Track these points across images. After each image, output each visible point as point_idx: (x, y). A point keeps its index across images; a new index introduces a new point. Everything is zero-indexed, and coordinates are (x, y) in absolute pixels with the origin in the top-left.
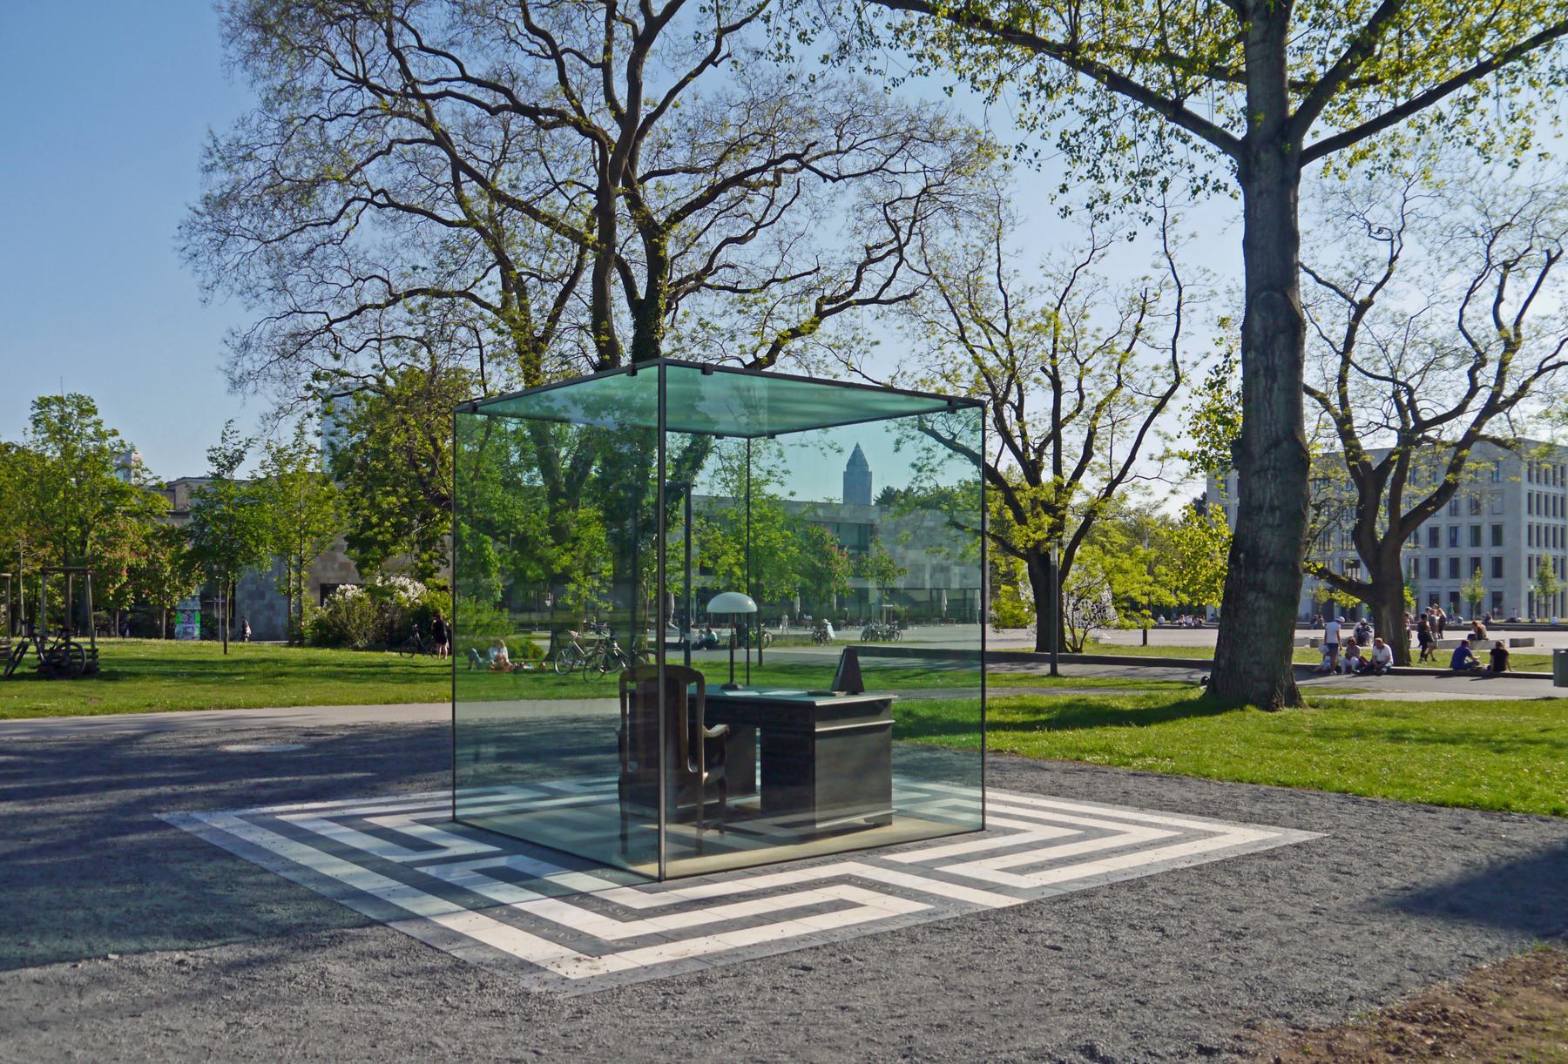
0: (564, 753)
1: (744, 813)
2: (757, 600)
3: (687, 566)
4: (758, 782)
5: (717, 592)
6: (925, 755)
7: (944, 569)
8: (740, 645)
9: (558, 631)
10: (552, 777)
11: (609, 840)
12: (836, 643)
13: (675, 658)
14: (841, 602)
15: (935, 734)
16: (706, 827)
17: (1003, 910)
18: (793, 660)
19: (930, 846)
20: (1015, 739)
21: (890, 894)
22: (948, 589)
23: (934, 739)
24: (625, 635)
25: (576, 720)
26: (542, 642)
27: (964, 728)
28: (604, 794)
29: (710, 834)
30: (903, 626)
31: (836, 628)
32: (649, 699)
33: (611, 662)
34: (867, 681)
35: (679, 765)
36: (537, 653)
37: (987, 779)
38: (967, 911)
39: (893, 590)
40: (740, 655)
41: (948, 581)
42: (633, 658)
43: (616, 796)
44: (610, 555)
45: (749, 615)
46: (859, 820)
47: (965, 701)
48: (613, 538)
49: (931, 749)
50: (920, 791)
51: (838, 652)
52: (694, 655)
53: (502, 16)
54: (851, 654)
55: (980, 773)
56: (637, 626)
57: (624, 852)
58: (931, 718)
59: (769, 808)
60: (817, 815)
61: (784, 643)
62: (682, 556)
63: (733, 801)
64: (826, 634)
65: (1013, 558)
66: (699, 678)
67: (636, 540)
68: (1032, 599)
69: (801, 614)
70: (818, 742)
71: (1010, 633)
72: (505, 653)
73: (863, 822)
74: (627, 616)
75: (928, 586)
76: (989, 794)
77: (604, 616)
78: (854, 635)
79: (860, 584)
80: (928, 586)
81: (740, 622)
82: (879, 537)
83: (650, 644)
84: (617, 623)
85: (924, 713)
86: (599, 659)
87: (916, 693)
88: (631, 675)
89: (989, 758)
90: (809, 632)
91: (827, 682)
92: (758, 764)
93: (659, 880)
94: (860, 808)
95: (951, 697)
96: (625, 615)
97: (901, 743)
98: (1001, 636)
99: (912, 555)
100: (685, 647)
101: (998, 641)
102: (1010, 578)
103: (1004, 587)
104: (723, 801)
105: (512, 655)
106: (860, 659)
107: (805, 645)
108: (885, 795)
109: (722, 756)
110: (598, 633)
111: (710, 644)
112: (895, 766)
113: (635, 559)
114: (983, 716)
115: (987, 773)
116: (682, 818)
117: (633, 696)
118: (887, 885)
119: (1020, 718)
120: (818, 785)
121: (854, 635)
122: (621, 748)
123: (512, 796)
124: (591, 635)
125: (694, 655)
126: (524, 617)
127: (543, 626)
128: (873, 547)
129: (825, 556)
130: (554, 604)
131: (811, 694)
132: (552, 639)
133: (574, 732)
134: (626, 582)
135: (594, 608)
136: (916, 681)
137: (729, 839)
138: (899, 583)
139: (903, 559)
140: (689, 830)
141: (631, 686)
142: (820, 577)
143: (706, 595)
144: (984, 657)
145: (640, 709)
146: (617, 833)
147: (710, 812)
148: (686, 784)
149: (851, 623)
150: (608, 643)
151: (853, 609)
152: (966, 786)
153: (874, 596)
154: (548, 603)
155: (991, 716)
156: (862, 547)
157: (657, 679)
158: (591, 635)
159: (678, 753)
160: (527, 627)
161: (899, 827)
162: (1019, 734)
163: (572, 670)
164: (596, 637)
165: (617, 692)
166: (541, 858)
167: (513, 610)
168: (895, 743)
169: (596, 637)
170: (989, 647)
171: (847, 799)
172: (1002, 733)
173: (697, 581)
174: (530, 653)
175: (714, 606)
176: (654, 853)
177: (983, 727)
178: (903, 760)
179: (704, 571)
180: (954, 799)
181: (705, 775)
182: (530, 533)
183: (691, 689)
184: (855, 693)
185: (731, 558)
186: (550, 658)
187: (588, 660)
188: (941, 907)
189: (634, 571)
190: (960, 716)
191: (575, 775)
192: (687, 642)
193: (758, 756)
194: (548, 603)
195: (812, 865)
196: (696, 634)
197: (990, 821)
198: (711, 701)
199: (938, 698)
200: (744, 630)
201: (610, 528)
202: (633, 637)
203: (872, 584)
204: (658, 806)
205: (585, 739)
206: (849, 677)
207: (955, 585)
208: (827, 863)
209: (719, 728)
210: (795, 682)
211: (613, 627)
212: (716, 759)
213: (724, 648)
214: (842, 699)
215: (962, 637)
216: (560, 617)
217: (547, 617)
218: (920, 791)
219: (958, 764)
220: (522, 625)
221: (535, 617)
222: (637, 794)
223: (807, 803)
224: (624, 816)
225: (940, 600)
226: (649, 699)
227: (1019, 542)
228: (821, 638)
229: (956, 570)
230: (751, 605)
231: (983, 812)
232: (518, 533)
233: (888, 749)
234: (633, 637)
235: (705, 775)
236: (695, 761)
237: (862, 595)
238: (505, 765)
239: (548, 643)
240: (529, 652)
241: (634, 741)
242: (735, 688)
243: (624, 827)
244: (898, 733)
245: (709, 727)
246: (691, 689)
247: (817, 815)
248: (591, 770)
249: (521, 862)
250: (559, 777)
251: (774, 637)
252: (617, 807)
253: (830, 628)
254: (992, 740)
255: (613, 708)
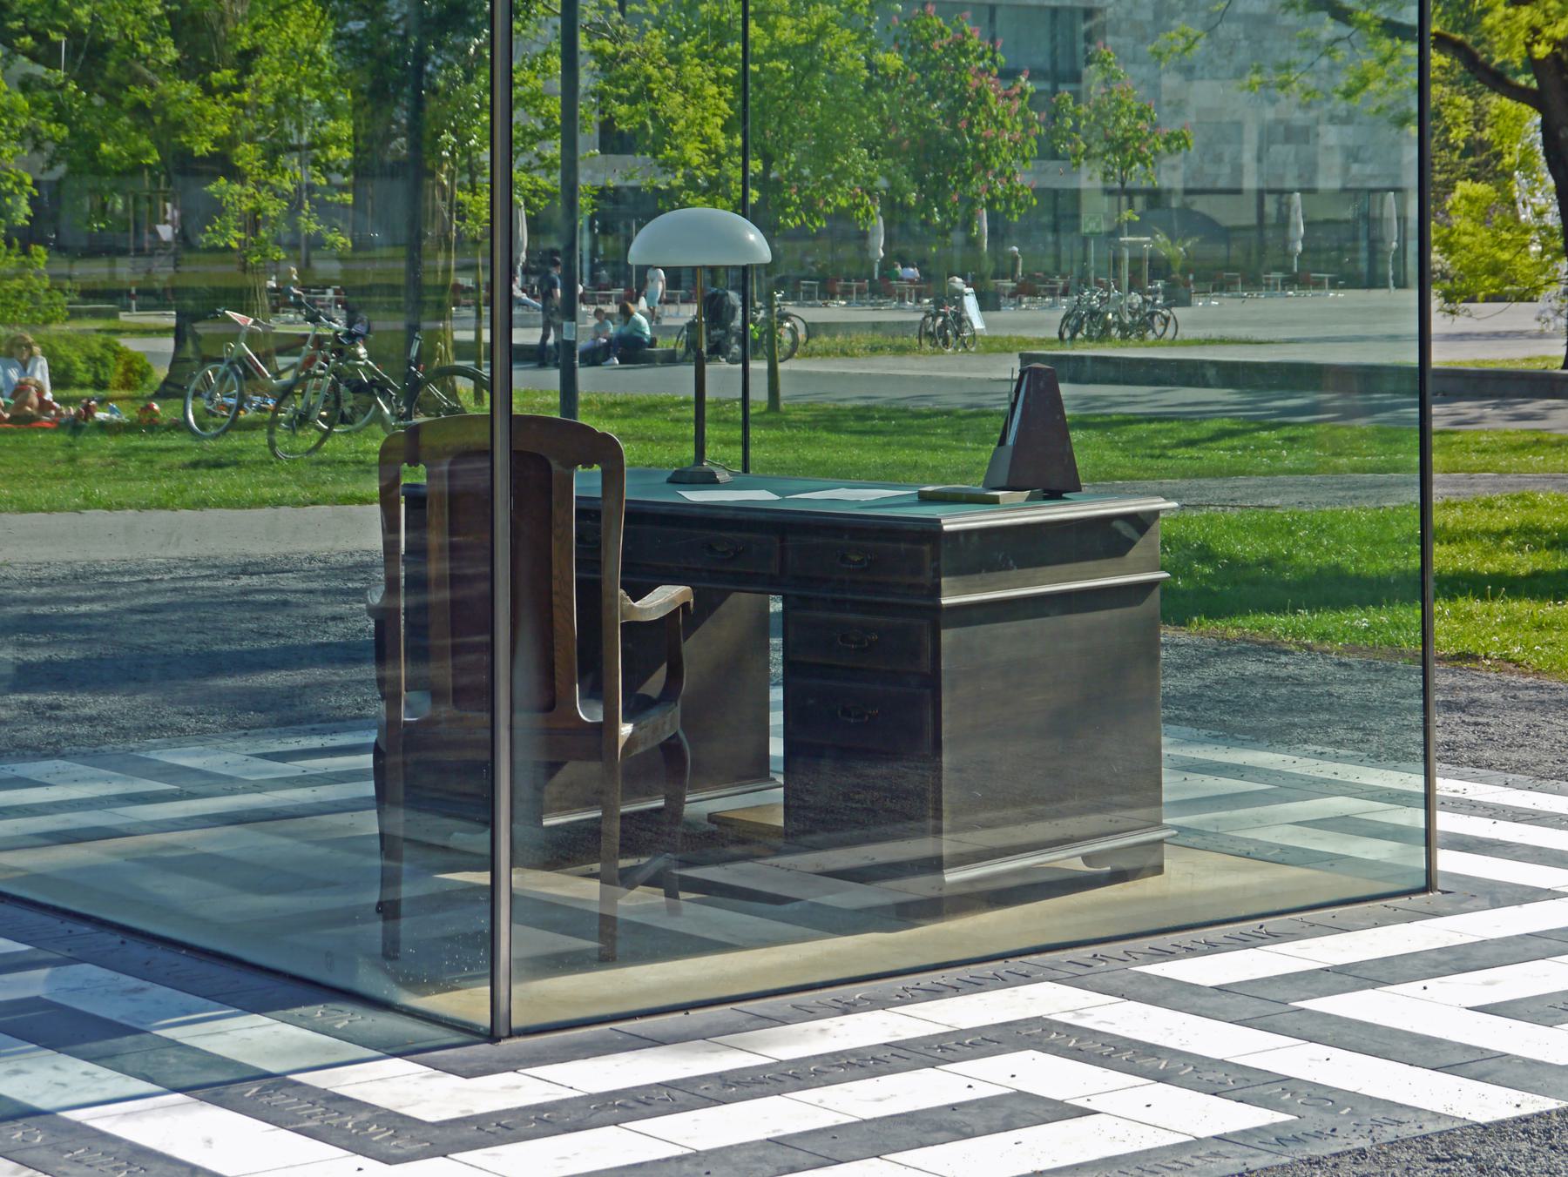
0: (213, 664)
1: (727, 838)
2: (769, 230)
3: (569, 130)
4: (776, 748)
5: (669, 199)
6: (1253, 667)
7: (1298, 135)
8: (717, 350)
9: (195, 310)
10: (178, 735)
11: (348, 917)
12: (993, 346)
13: (536, 391)
14: (998, 232)
15: (1279, 609)
16: (627, 879)
17: (1498, 1129)
18: (865, 408)
19: (1277, 937)
20: (1512, 623)
21: (1162, 1078)
22: (1308, 191)
23: (1278, 623)
24: (390, 323)
25: (246, 569)
26: (151, 343)
27: (1372, 592)
28: (321, 783)
29: (639, 902)
30: (1177, 297)
31: (987, 302)
32: (467, 508)
33: (350, 399)
34: (1087, 450)
35: (552, 703)
36: (134, 372)
37: (1439, 736)
38: (1390, 1133)
39: (1155, 197)
40: (722, 376)
41: (1310, 167)
42: (413, 393)
43: (369, 788)
44: (344, 98)
45: (744, 275)
46: (1070, 860)
47: (1363, 512)
48: (348, 45)
49: (1271, 649)
50: (1239, 771)
51: (1010, 368)
52: (585, 376)
53: (1367, 548)
54: (1040, 380)
55: (1425, 719)
56: (423, 299)
57: (390, 951)
58: (1268, 562)
59: (809, 823)
60: (948, 845)
61: (841, 351)
62: (554, 106)
63: (702, 804)
64: (960, 319)
65: (1497, 103)
66: (603, 451)
67: (421, 58)
68: (1553, 219)
69: (886, 265)
70: (947, 636)
71: (1486, 317)
72: (41, 372)
73: (1079, 866)
74: (397, 270)
75: (1250, 183)
76: (1446, 786)
77: (326, 267)
78: (1039, 323)
79: (1055, 177)
80: (1250, 183)
81: (716, 295)
82: (1107, 47)
83: (461, 350)
84: (366, 290)
85: (1248, 548)
86: (313, 397)
87: (1217, 488)
88: (410, 446)
89: (1442, 678)
90: (911, 313)
91: (974, 458)
92: (777, 695)
93: (492, 1036)
94: (1070, 825)
95: (1335, 500)
96: (389, 266)
97: (1181, 636)
98: (1461, 324)
99: (1204, 93)
100: (561, 357)
101: (1471, 337)
102: (1484, 161)
103: (1464, 187)
104: (675, 802)
105: (61, 379)
106: (1065, 389)
107: (901, 350)
108: (1143, 785)
109: (675, 674)
110: (314, 319)
111: (631, 350)
112: (1169, 700)
113: (418, 104)
114: (1425, 555)
115: (1437, 719)
116: (565, 851)
117: (417, 501)
118: (1153, 1050)
119: (1526, 562)
120: (946, 759)
121: (1039, 323)
122: (382, 650)
123: (67, 787)
124: (291, 324)
125: (585, 376)
126: (95, 271)
127: (152, 298)
128: (1093, 77)
129: (962, 103)
130: (185, 239)
131: (926, 499)
132: (180, 334)
133: (243, 602)
134: (398, 167)
135: (306, 248)
136: (1219, 454)
137: (694, 914)
138: (1170, 177)
139: (1179, 107)
140: (578, 888)
141: (415, 476)
142: (938, 160)
143: (624, 211)
144: (1425, 383)
145: (436, 538)
146: (374, 897)
147: (640, 834)
148: (568, 744)
149: (1027, 289)
150: (341, 348)
151: (1039, 248)
152: (1376, 759)
153: (1095, 216)
154: (166, 232)
155: (1444, 558)
156: (1063, 75)
157: (489, 453)
158: (291, 324)
159: (548, 669)
160: (109, 297)
161: (1186, 877)
162: (1522, 607)
163: (235, 425)
164: (308, 328)
165: (373, 487)
166: (146, 973)
167: (59, 249)
168: (1168, 633)
169: (308, 328)
170: (1440, 357)
171: (1040, 796)
172: (1476, 606)
173: (600, 172)
174: (114, 375)
175: (648, 245)
176: (477, 954)
177: (1423, 587)
178: (1189, 682)
179: (614, 141)
180: (1343, 797)
181: (626, 730)
182: (112, 33)
183: (586, 481)
184: (1054, 495)
185: (701, 116)
186: (171, 389)
187: (286, 393)
188: (1315, 1119)
189: (415, 146)
190: (1352, 559)
191: (248, 730)
192: (570, 346)
193: (777, 670)
194: (166, 232)
195: (935, 993)
196: (587, 325)
197: (1448, 861)
198: (639, 516)
199: (1284, 502)
200: (724, 311)
201: (339, 17)
202: (413, 328)
203: (1089, 179)
204: (492, 824)
205: (278, 620)
206: (1037, 444)
207: (1328, 181)
208: (977, 986)
209: (662, 599)
210: (874, 458)
211: (354, 300)
212: (655, 684)
213: (670, 359)
214: (1018, 511)
215: (1360, 327)
216: (202, 274)
217: (163, 273)
218: (1239, 771)
219: (1351, 692)
220: (89, 294)
221: (125, 271)
222: (430, 778)
223: (916, 808)
224: (388, 844)
225: (1284, 222)
226: (467, 508)
227: (1507, 52)
228: (946, 331)
229: (1331, 135)
230: (756, 244)
231: (1429, 838)
232: (75, 34)
233: (1150, 649)
234: (413, 328)
235: (626, 730)
236: (597, 690)
237: (1061, 209)
238: (42, 699)
239: (168, 344)
240: (110, 371)
241: (428, 625)
242: (709, 481)
243: (389, 879)
244: (1180, 606)
245: (637, 593)
246: (586, 481)
247: (948, 845)
248: (287, 714)
249: (88, 986)
250: (202, 735)
251: (812, 329)
252: (369, 824)
253: (971, 303)
254: (1453, 623)
255: (361, 532)
